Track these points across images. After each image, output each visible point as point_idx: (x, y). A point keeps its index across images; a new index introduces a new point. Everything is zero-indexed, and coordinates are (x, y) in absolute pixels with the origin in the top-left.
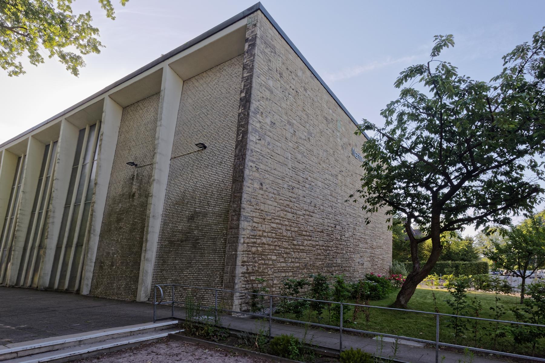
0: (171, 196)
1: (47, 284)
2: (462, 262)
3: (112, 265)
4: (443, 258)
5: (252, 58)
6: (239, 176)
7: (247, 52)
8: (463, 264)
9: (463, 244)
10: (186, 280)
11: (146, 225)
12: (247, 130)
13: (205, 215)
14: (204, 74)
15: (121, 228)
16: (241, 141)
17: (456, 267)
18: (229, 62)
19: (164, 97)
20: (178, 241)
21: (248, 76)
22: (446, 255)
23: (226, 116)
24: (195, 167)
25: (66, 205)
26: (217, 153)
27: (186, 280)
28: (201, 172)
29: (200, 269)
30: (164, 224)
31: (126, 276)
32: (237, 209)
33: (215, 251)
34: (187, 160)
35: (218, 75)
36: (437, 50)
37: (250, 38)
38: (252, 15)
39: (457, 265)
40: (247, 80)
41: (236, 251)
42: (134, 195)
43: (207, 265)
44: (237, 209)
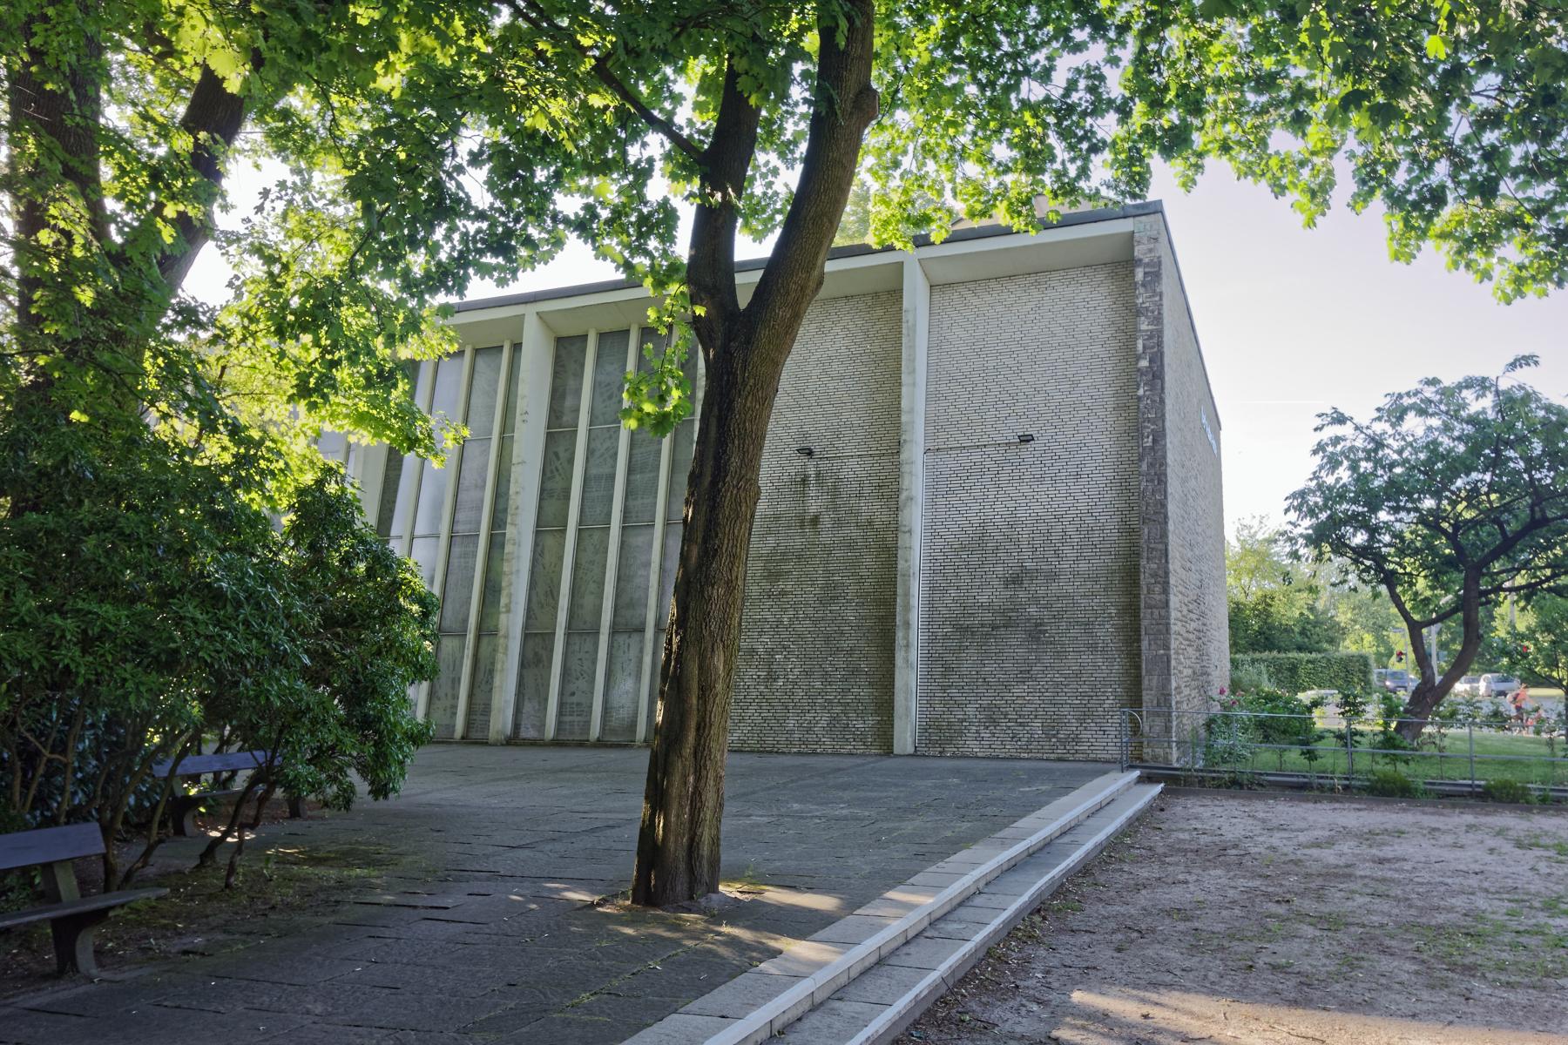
0: (943, 532)
1: (509, 729)
2: (1304, 656)
3: (772, 677)
4: (1252, 644)
5: (1157, 298)
6: (1155, 513)
7: (1143, 285)
8: (1308, 662)
9: (1302, 602)
10: (1022, 706)
11: (899, 591)
12: (1164, 429)
13: (1053, 576)
14: (993, 284)
15: (783, 593)
16: (1152, 448)
17: (1289, 670)
18: (1062, 273)
19: (915, 325)
20: (983, 626)
21: (1152, 331)
22: (1260, 633)
23: (1075, 384)
24: (1004, 477)
25: (538, 525)
26: (1065, 455)
27: (1022, 706)
28: (1025, 489)
29: (1057, 684)
30: (932, 589)
31: (830, 702)
32: (1161, 573)
33: (1093, 648)
34: (976, 457)
35: (1035, 293)
36: (1514, 365)
37: (1146, 260)
38: (1143, 218)
39: (1293, 664)
40: (1150, 337)
41: (1167, 648)
42: (815, 520)
43: (1078, 675)
44: (1161, 573)
